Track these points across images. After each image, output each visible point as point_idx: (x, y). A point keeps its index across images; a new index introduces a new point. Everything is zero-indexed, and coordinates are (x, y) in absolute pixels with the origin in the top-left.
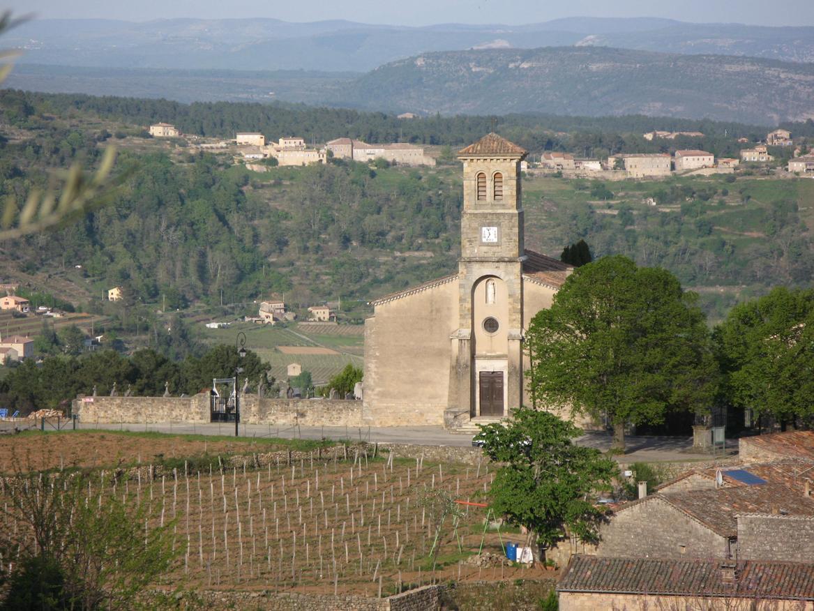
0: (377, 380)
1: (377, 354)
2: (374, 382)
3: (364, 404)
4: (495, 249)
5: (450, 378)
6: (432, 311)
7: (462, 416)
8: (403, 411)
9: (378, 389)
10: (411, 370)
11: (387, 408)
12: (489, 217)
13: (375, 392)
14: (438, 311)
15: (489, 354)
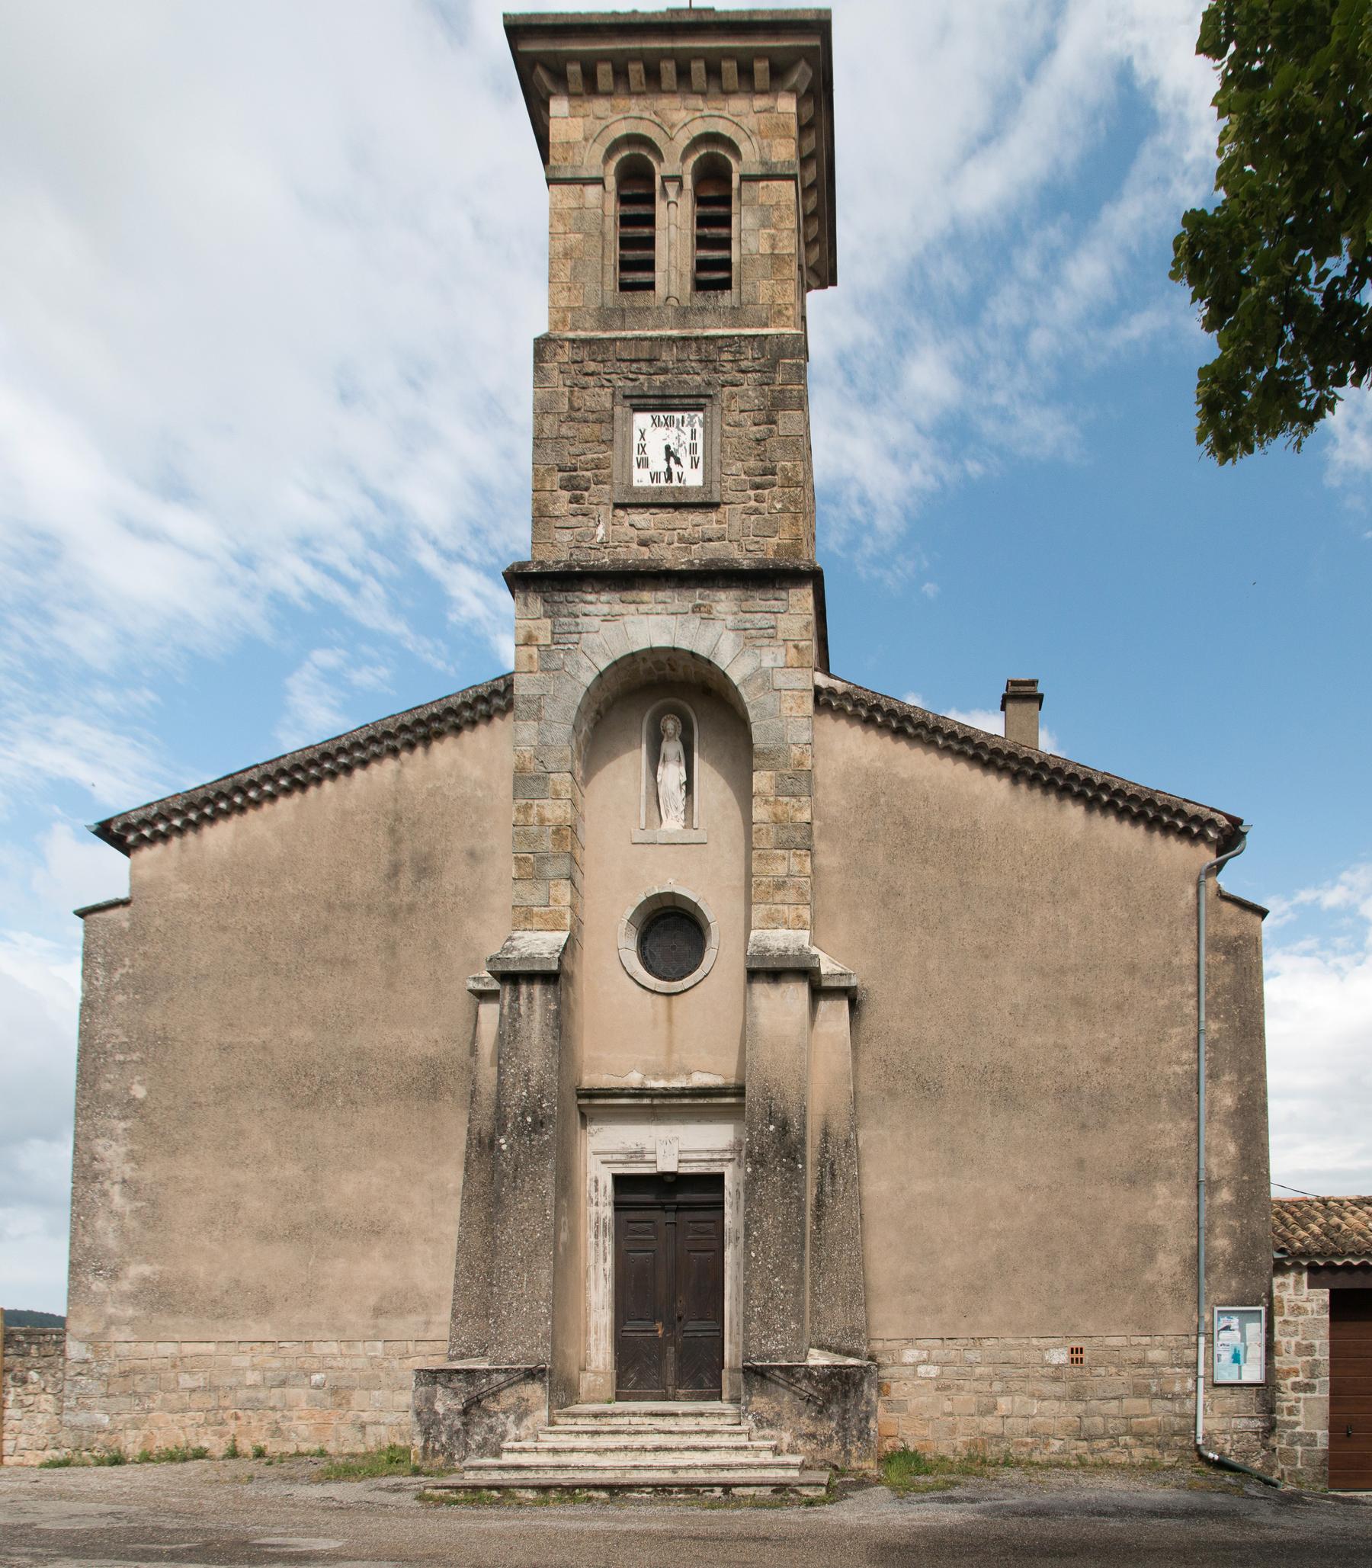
0: (131, 1223)
1: (139, 1092)
2: (123, 1233)
3: (74, 1349)
4: (690, 522)
5: (467, 1202)
6: (395, 871)
7: (508, 1398)
8: (252, 1378)
9: (137, 1270)
10: (292, 1171)
11: (177, 1363)
12: (668, 357)
13: (125, 1286)
14: (425, 868)
15: (660, 1084)
